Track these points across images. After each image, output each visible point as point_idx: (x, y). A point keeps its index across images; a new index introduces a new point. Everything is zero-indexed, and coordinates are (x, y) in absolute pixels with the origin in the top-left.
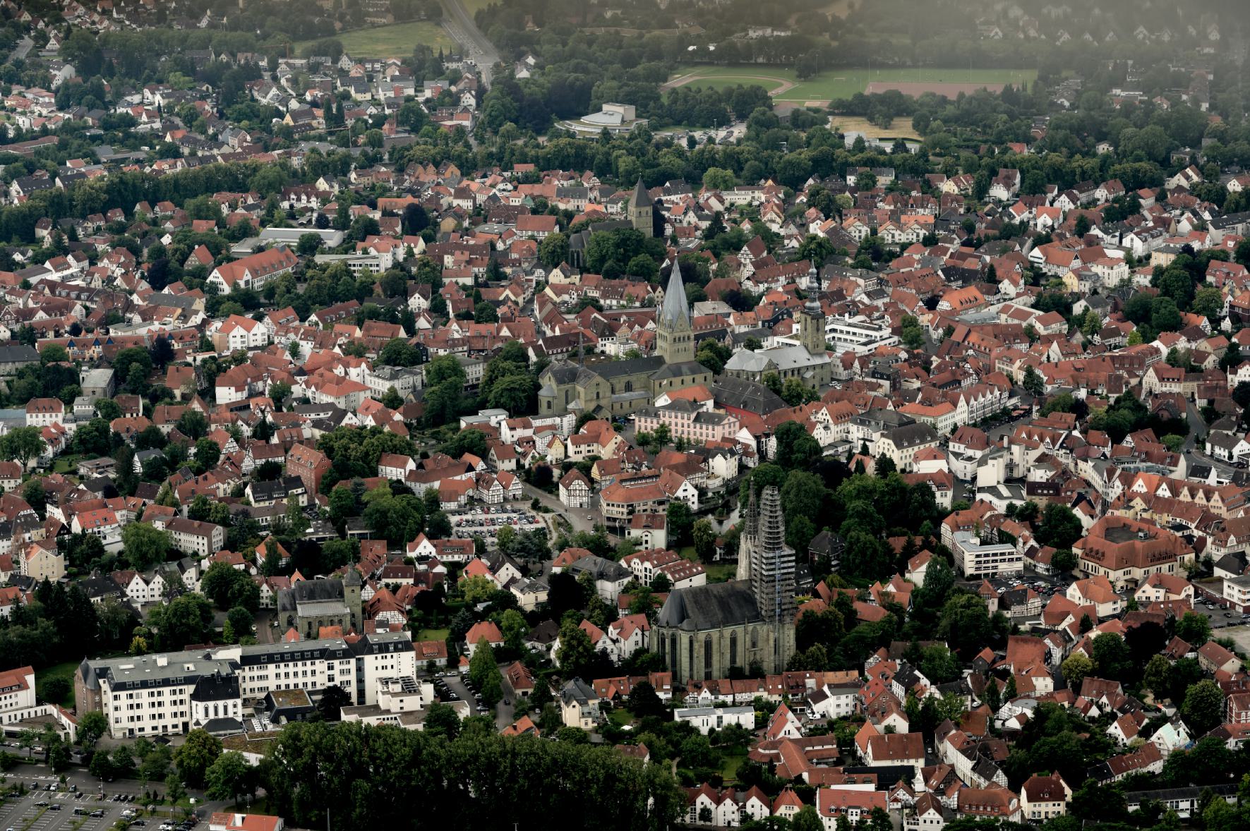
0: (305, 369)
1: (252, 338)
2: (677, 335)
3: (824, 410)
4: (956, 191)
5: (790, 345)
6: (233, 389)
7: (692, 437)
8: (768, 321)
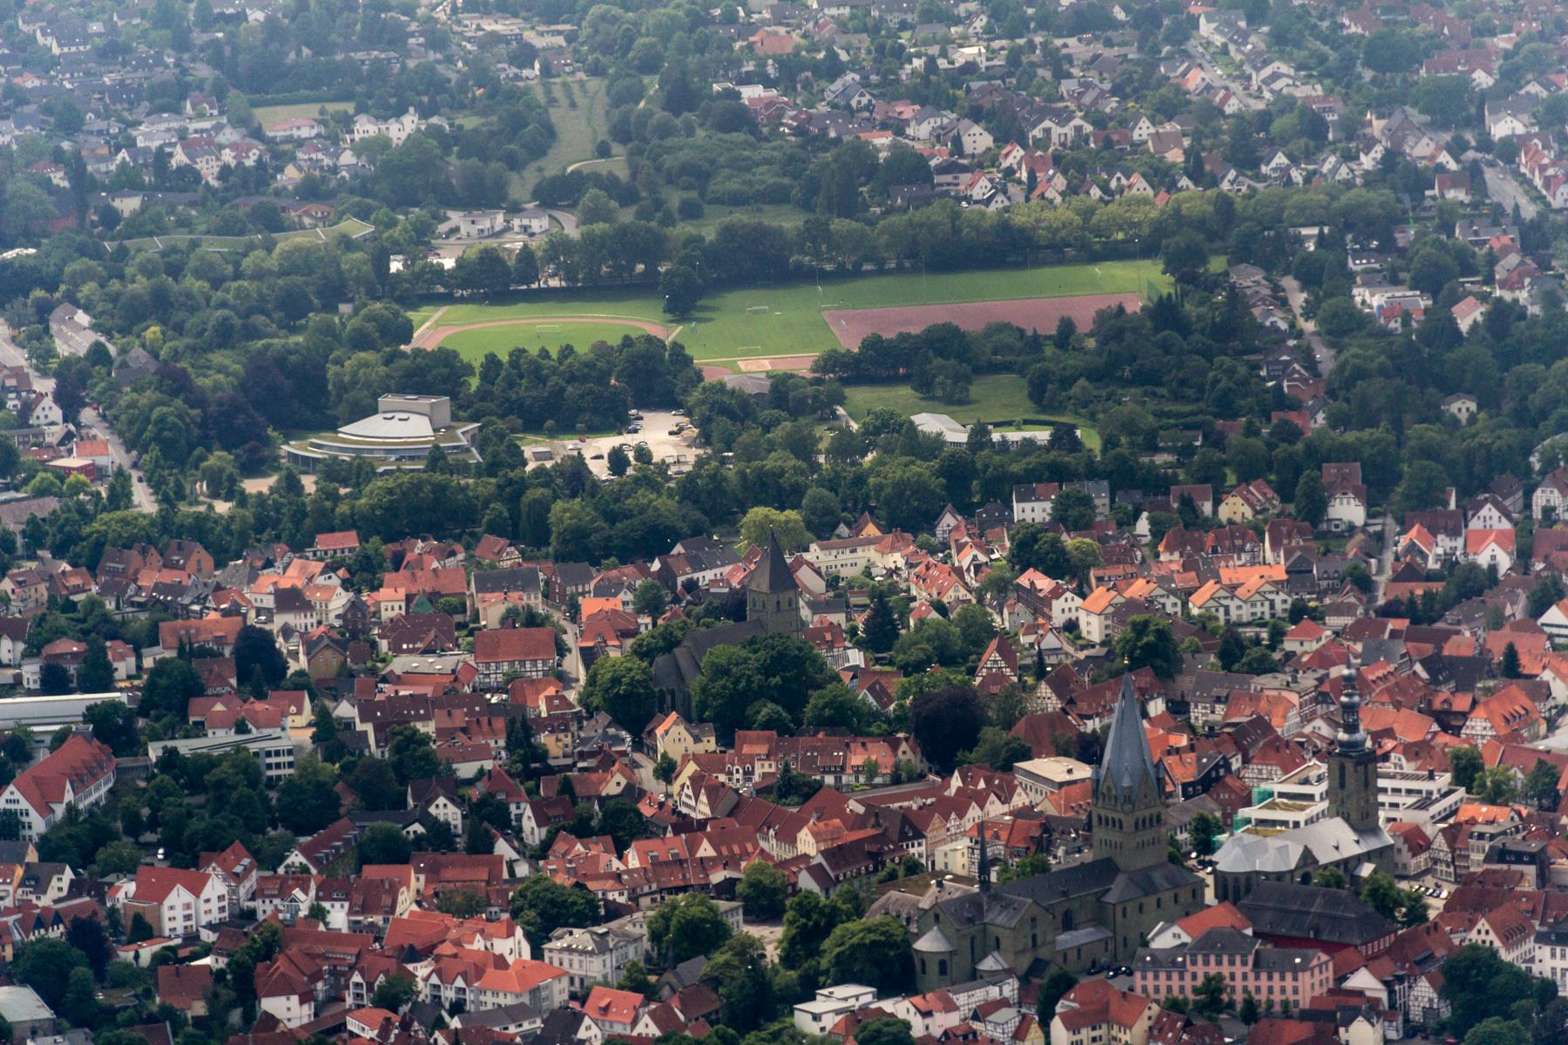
0: (418, 947)
1: (204, 907)
2: (1140, 815)
3: (1483, 924)
4: (1249, 513)
5: (1274, 823)
6: (295, 999)
7: (1277, 997)
8: (1190, 784)
